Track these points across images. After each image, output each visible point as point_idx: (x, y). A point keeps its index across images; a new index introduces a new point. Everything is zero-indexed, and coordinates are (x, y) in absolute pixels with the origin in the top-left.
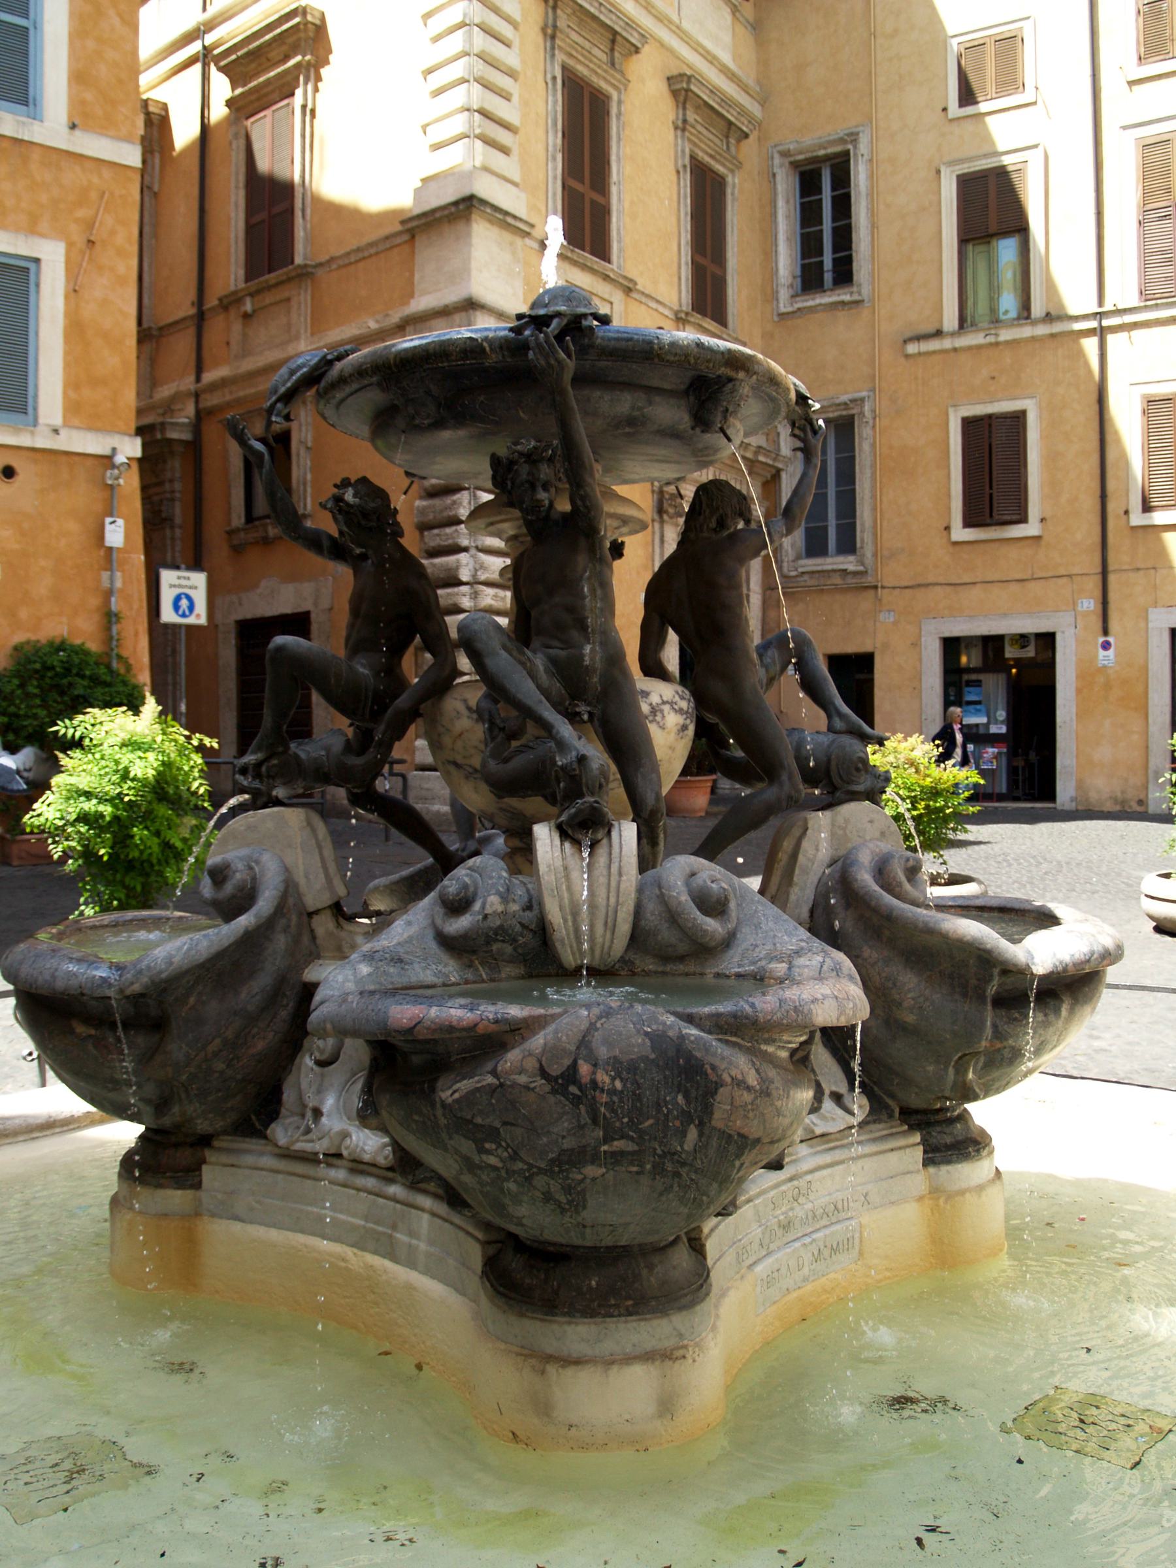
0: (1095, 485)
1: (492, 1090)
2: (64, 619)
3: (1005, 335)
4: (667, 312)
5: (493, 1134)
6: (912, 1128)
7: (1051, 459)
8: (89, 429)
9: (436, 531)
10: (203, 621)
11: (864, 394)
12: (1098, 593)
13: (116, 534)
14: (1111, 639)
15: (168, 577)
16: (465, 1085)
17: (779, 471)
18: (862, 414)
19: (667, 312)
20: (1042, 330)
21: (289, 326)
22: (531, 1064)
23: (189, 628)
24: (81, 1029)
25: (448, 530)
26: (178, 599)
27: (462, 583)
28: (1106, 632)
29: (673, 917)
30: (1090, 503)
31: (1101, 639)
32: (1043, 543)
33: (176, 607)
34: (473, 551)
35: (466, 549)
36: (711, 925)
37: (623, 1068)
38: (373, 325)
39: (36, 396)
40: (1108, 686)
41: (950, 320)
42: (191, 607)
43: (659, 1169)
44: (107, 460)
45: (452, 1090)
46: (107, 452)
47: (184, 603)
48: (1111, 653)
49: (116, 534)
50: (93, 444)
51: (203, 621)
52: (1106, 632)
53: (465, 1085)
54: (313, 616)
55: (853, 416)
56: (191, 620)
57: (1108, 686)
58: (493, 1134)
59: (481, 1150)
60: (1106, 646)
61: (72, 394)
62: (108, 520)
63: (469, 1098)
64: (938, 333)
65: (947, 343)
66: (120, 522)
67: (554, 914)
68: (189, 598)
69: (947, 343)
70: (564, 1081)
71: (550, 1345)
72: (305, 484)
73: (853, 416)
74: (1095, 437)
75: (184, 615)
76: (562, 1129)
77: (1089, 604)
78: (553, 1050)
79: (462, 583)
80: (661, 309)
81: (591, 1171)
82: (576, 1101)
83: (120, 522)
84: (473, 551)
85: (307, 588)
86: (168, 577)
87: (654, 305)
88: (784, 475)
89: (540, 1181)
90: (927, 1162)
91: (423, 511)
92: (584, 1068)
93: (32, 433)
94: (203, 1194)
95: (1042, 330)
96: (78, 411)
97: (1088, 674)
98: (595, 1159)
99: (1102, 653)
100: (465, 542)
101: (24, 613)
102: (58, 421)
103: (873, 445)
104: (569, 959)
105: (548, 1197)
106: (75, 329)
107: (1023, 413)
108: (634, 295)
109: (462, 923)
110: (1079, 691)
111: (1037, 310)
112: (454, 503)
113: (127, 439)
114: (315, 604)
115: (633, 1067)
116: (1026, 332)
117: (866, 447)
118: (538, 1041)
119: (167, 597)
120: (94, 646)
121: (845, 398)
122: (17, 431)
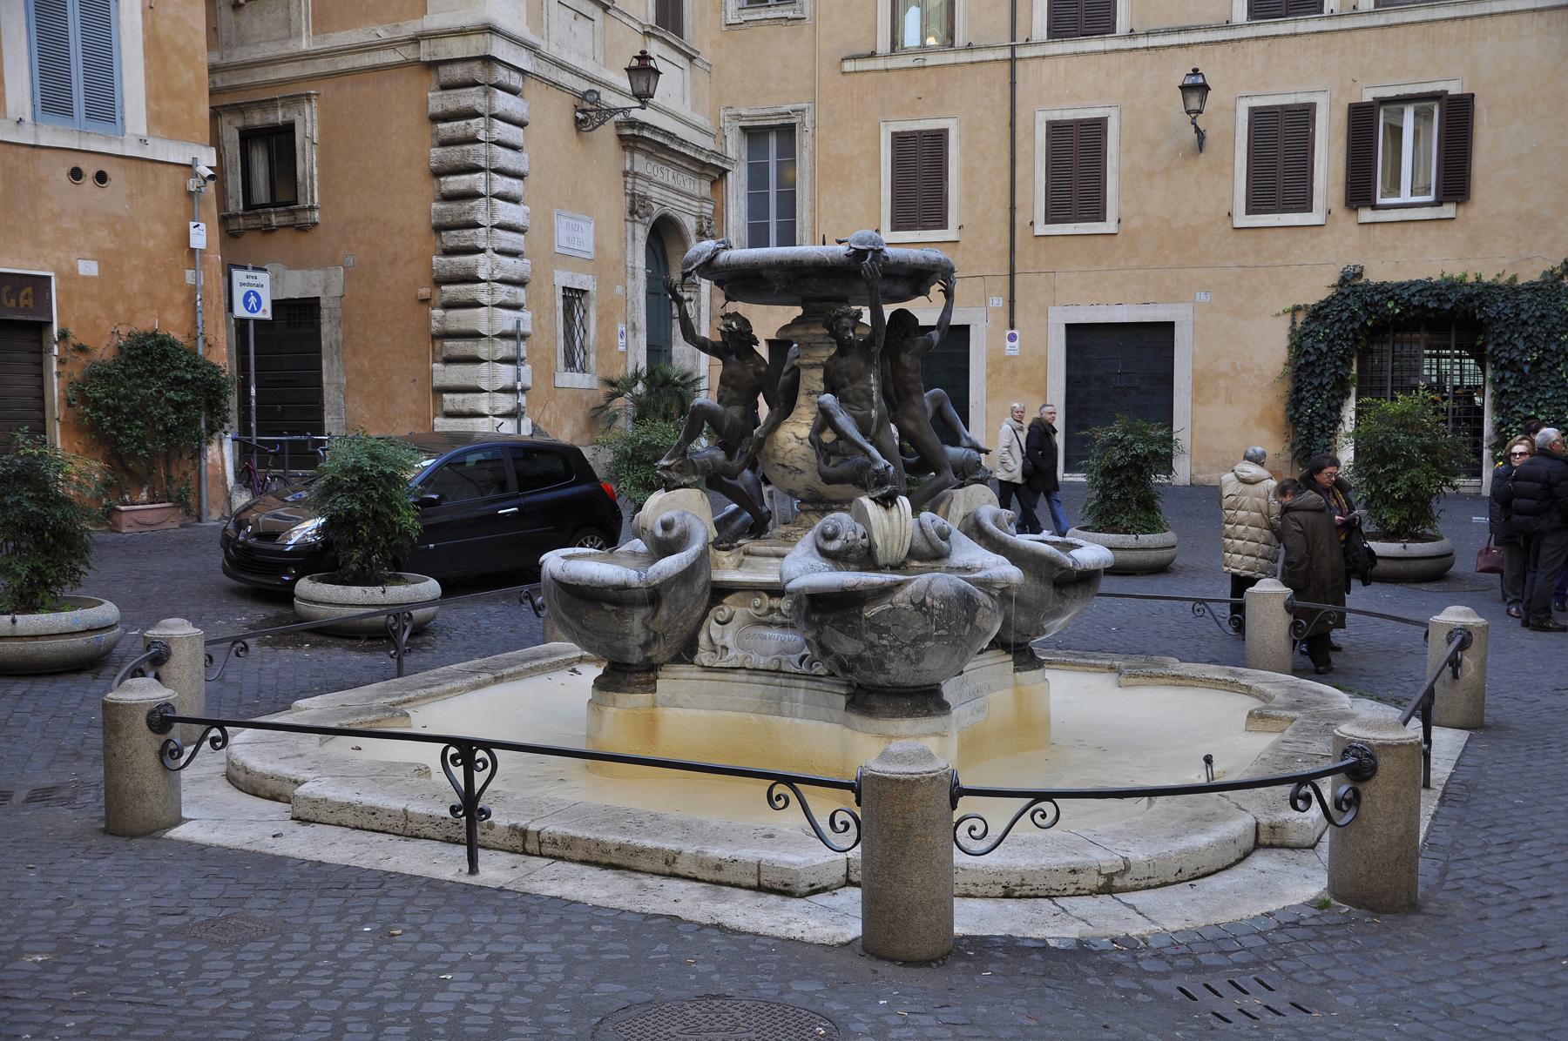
0: (1006, 198)
1: (890, 610)
2: (155, 313)
3: (931, 60)
4: (636, 26)
5: (888, 630)
6: (1009, 652)
7: (969, 172)
8: (171, 138)
9: (454, 233)
10: (268, 316)
11: (805, 105)
12: (1006, 292)
13: (199, 237)
14: (1016, 332)
15: (239, 276)
16: (877, 609)
17: (726, 171)
18: (803, 123)
19: (636, 26)
20: (964, 57)
21: (288, 21)
22: (907, 599)
23: (257, 321)
24: (607, 607)
25: (467, 233)
26: (247, 296)
27: (480, 281)
28: (1012, 327)
29: (928, 540)
30: (1002, 214)
31: (1009, 332)
32: (960, 246)
33: (246, 304)
34: (490, 252)
35: (483, 251)
36: (944, 544)
37: (945, 600)
38: (385, 35)
39: (122, 107)
40: (1013, 372)
41: (883, 45)
42: (259, 303)
43: (954, 642)
44: (190, 168)
45: (870, 612)
46: (188, 161)
47: (253, 299)
48: (1016, 344)
49: (199, 237)
50: (177, 153)
51: (268, 316)
52: (1012, 327)
53: (877, 609)
54: (323, 302)
55: (794, 125)
56: (259, 315)
57: (1013, 372)
58: (888, 630)
59: (880, 638)
60: (1012, 338)
61: (154, 107)
62: (192, 224)
63: (878, 615)
64: (873, 55)
65: (879, 64)
66: (203, 226)
67: (878, 539)
68: (256, 295)
69: (879, 64)
70: (920, 606)
71: (892, 731)
72: (312, 178)
73: (794, 125)
74: (1006, 156)
75: (253, 311)
76: (918, 627)
77: (999, 302)
78: (916, 593)
79: (480, 281)
80: (632, 24)
81: (929, 644)
82: (925, 614)
83: (203, 226)
84: (490, 252)
85: (316, 276)
86: (239, 276)
87: (625, 20)
88: (729, 175)
89: (905, 650)
90: (1015, 671)
91: (440, 214)
92: (928, 600)
93: (122, 142)
94: (657, 695)
95: (964, 57)
96: (158, 121)
97: (997, 364)
98: (930, 639)
99: (1009, 344)
100: (482, 245)
101: (120, 308)
102: (143, 131)
103: (813, 153)
104: (881, 560)
105: (908, 657)
106: (154, 44)
107: (946, 131)
108: (611, 12)
109: (834, 545)
110: (989, 376)
111: (960, 39)
112: (473, 208)
113: (203, 149)
114: (325, 291)
115: (948, 599)
116: (950, 58)
117: (806, 154)
118: (909, 589)
119: (238, 294)
120: (179, 337)
121: (786, 108)
122: (108, 139)
